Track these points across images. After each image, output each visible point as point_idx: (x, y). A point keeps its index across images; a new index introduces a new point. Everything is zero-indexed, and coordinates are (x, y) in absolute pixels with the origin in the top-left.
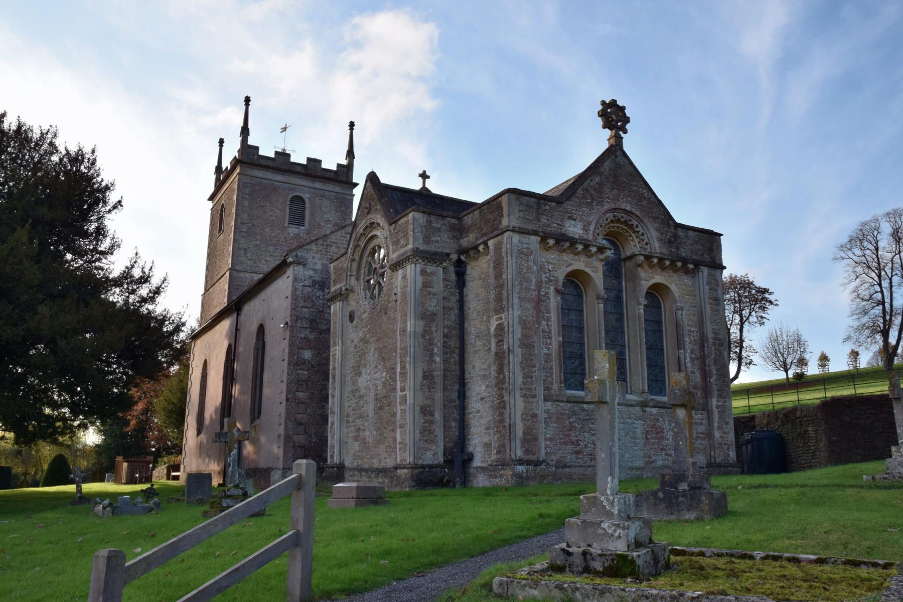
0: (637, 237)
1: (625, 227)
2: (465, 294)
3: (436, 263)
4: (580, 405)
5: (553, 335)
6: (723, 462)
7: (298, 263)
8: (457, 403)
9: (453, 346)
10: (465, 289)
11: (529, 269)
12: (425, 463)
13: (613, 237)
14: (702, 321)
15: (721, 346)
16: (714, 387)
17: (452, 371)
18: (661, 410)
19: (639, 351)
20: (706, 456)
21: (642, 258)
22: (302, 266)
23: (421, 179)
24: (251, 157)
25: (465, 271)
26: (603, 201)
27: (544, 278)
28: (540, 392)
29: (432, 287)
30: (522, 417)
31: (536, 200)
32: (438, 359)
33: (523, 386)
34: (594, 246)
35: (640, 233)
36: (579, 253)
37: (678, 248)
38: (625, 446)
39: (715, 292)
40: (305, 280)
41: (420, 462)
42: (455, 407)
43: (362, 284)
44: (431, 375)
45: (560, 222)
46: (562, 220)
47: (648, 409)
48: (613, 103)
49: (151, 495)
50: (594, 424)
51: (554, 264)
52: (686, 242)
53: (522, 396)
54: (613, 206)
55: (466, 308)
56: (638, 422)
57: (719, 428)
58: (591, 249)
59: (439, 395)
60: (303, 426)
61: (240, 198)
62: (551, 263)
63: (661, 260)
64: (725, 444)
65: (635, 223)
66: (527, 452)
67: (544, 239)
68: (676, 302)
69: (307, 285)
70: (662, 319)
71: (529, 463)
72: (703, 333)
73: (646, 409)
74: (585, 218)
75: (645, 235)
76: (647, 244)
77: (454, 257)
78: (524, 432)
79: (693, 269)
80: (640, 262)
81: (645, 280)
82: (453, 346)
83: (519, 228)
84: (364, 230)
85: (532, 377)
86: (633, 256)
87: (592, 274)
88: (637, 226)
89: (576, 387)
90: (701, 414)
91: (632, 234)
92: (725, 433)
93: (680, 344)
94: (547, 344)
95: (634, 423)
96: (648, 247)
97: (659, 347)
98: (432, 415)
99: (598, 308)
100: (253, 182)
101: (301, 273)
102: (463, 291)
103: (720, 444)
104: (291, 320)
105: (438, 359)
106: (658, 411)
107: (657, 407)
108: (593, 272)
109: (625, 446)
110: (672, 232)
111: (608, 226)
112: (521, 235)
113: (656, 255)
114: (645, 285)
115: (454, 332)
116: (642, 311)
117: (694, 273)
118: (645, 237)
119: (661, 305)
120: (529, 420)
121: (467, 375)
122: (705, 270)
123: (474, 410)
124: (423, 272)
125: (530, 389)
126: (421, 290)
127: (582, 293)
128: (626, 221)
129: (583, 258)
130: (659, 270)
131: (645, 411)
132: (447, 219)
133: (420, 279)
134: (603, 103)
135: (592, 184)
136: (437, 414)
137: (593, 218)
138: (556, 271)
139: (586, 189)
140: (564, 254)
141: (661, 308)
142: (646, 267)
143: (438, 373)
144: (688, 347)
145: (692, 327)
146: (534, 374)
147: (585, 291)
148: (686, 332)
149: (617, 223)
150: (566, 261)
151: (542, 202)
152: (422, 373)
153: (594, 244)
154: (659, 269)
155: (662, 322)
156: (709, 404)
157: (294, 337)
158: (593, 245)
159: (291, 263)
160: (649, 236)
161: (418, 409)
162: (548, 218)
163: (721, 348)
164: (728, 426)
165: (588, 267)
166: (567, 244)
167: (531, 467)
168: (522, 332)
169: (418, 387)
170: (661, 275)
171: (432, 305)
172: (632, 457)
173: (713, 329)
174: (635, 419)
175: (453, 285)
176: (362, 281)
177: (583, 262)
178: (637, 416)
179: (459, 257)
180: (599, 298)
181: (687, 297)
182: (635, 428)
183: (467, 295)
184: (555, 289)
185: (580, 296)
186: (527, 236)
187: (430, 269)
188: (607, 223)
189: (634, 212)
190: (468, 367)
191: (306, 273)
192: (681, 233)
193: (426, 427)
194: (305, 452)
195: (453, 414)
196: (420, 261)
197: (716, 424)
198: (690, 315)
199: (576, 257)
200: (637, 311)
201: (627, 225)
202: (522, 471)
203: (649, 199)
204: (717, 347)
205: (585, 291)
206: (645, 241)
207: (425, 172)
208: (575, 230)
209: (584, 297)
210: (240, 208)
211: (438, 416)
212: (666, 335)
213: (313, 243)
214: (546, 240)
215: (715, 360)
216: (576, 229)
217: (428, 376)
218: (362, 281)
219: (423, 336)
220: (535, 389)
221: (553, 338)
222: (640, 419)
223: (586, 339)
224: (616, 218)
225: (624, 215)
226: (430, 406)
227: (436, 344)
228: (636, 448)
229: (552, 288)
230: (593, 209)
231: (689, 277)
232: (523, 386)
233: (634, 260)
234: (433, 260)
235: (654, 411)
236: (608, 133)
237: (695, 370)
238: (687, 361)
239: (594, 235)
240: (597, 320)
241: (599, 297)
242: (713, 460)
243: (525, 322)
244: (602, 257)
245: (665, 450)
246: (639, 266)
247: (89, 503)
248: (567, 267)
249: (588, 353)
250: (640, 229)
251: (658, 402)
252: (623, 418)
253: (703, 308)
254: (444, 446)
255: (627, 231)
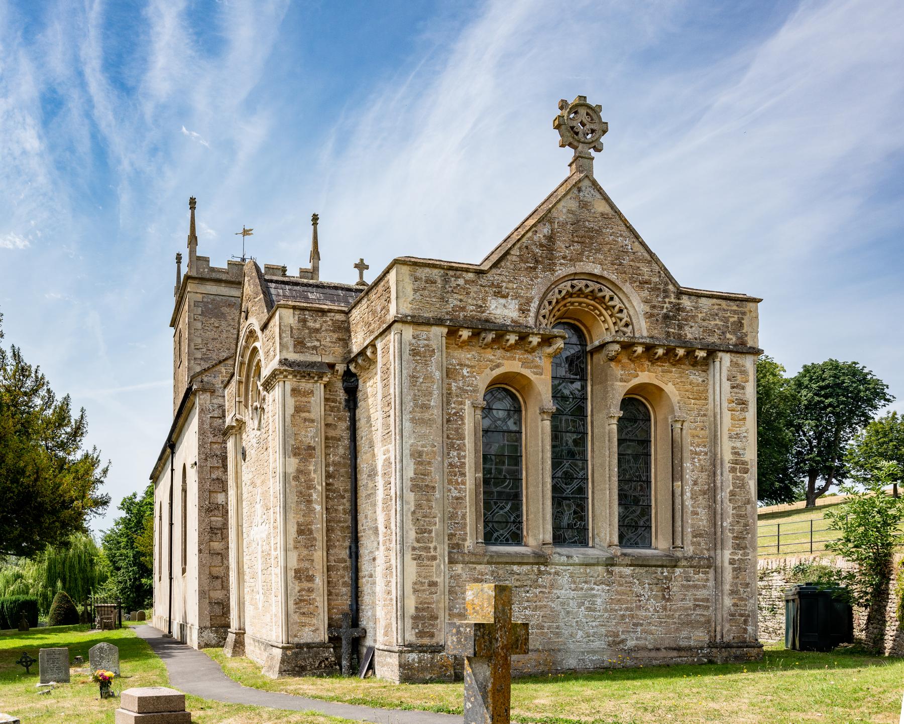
0: (611, 316)
1: (592, 302)
2: (357, 419)
3: (313, 378)
4: (508, 567)
5: (467, 470)
6: (736, 640)
7: (204, 390)
8: (348, 564)
9: (341, 488)
10: (357, 411)
11: (428, 377)
12: (302, 641)
13: (575, 319)
14: (715, 436)
15: (746, 473)
16: (729, 534)
17: (340, 522)
18: (638, 570)
19: (607, 486)
20: (709, 631)
21: (617, 347)
22: (208, 394)
23: (357, 271)
24: (201, 270)
25: (357, 387)
26: (555, 264)
27: (454, 388)
28: (442, 550)
29: (309, 412)
30: (413, 588)
31: (442, 272)
32: (318, 508)
33: (417, 545)
34: (536, 334)
35: (617, 309)
36: (638, 357)
37: (680, 327)
38: (577, 622)
39: (742, 391)
40: (214, 410)
41: (296, 640)
42: (345, 568)
43: (250, 412)
44: (309, 529)
45: (480, 303)
46: (484, 300)
47: (616, 569)
48: (583, 102)
49: (29, 663)
50: (528, 592)
51: (471, 367)
52: (693, 317)
53: (415, 559)
54: (572, 270)
55: (358, 438)
56: (599, 587)
57: (733, 592)
58: (530, 339)
59: (319, 555)
60: (220, 581)
61: (192, 320)
62: (468, 366)
63: (649, 348)
64: (741, 615)
65: (607, 293)
66: (421, 634)
67: (452, 333)
68: (672, 411)
69: (216, 416)
70: (650, 437)
71: (421, 649)
72: (715, 455)
73: (613, 568)
74: (522, 293)
75: (625, 311)
76: (627, 325)
77: (341, 368)
78: (416, 608)
79: (704, 358)
80: (613, 353)
81: (622, 380)
82: (341, 488)
83: (413, 317)
84: (246, 342)
85: (430, 532)
86: (602, 346)
87: (532, 377)
88: (611, 299)
89: (507, 540)
90: (706, 573)
91: (604, 312)
92: (741, 599)
93: (676, 473)
94: (458, 484)
95: (593, 589)
96: (628, 330)
97: (644, 478)
98: (310, 579)
99: (542, 427)
100: (205, 300)
101: (208, 402)
102: (355, 415)
103: (733, 615)
104: (199, 460)
105: (318, 508)
106: (634, 570)
107: (631, 566)
108: (536, 373)
109: (577, 622)
110: (670, 303)
111: (563, 303)
112: (416, 327)
113: (641, 341)
114: (620, 389)
115: (343, 470)
116: (615, 427)
117: (707, 365)
118: (624, 315)
119: (650, 417)
120: (424, 590)
121: (360, 528)
122: (726, 359)
123: (366, 573)
124: (295, 391)
125: (427, 549)
126: (293, 416)
127: (520, 407)
128: (592, 292)
129: (519, 354)
130: (647, 363)
131: (610, 573)
132: (329, 314)
133: (291, 402)
134: (563, 105)
135: (536, 238)
136: (317, 579)
137: (536, 293)
138: (474, 377)
139: (527, 247)
140: (489, 350)
141: (650, 420)
142: (625, 360)
143: (319, 527)
144: (688, 476)
145: (698, 446)
146: (434, 528)
147: (525, 402)
148: (686, 455)
149: (578, 296)
150: (491, 361)
151: (451, 273)
152: (296, 527)
153: (535, 331)
154: (647, 363)
155: (650, 441)
156: (719, 558)
157: (204, 479)
158: (533, 333)
159: (196, 391)
160: (631, 313)
161: (291, 574)
162: (461, 297)
163: (745, 475)
164: (749, 589)
165: (527, 368)
166: (491, 336)
167: (428, 656)
168: (415, 470)
169: (291, 544)
170: (649, 371)
171: (312, 435)
172: (589, 637)
173: (733, 448)
174: (595, 584)
175: (342, 406)
176: (250, 408)
177: (520, 360)
178: (599, 579)
179: (348, 367)
180: (544, 412)
181: (693, 401)
182: (594, 596)
183: (359, 419)
184: (472, 403)
185: (518, 411)
186: (425, 328)
187: (305, 385)
188: (559, 297)
189: (606, 276)
190: (361, 517)
191: (215, 401)
192: (686, 302)
193: (302, 596)
194: (223, 609)
195: (343, 577)
196: (290, 377)
197: (727, 587)
198: (695, 429)
199: (508, 354)
200: (607, 428)
201: (595, 298)
202: (413, 660)
203: (634, 253)
204: (739, 474)
205: (525, 402)
206: (624, 321)
207: (362, 260)
208: (506, 312)
209: (524, 412)
210: (193, 331)
211: (319, 582)
212: (656, 459)
213: (222, 365)
214: (458, 330)
215: (732, 494)
216: (507, 311)
217: (304, 530)
218: (250, 408)
219: (296, 478)
220: (435, 548)
221: (467, 474)
222: (602, 583)
223: (524, 473)
224: (577, 288)
225: (589, 283)
226: (307, 569)
227: (315, 488)
228: (594, 624)
229: (468, 402)
230: (536, 278)
231: (698, 371)
232: (417, 545)
233: (604, 352)
234: (309, 374)
235: (628, 571)
236: (569, 153)
237: (699, 510)
238: (685, 497)
239: (537, 317)
240: (540, 444)
241: (543, 412)
242: (719, 637)
243: (420, 454)
244: (550, 350)
245: (642, 625)
246: (612, 359)
247: (299, 583)
248: (492, 369)
249: (527, 493)
250: (616, 302)
251: (639, 558)
252: (575, 583)
253: (719, 417)
254: (330, 619)
255: (596, 308)
